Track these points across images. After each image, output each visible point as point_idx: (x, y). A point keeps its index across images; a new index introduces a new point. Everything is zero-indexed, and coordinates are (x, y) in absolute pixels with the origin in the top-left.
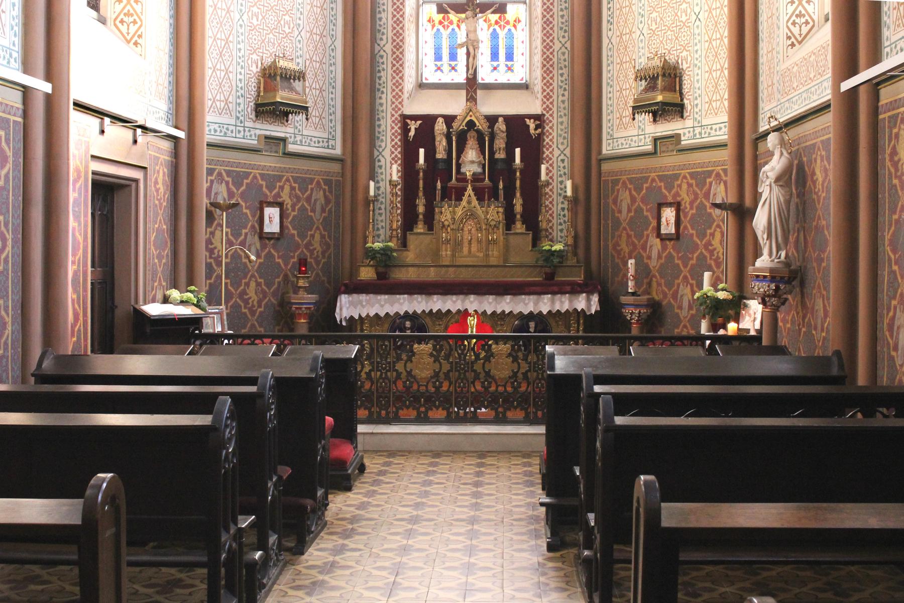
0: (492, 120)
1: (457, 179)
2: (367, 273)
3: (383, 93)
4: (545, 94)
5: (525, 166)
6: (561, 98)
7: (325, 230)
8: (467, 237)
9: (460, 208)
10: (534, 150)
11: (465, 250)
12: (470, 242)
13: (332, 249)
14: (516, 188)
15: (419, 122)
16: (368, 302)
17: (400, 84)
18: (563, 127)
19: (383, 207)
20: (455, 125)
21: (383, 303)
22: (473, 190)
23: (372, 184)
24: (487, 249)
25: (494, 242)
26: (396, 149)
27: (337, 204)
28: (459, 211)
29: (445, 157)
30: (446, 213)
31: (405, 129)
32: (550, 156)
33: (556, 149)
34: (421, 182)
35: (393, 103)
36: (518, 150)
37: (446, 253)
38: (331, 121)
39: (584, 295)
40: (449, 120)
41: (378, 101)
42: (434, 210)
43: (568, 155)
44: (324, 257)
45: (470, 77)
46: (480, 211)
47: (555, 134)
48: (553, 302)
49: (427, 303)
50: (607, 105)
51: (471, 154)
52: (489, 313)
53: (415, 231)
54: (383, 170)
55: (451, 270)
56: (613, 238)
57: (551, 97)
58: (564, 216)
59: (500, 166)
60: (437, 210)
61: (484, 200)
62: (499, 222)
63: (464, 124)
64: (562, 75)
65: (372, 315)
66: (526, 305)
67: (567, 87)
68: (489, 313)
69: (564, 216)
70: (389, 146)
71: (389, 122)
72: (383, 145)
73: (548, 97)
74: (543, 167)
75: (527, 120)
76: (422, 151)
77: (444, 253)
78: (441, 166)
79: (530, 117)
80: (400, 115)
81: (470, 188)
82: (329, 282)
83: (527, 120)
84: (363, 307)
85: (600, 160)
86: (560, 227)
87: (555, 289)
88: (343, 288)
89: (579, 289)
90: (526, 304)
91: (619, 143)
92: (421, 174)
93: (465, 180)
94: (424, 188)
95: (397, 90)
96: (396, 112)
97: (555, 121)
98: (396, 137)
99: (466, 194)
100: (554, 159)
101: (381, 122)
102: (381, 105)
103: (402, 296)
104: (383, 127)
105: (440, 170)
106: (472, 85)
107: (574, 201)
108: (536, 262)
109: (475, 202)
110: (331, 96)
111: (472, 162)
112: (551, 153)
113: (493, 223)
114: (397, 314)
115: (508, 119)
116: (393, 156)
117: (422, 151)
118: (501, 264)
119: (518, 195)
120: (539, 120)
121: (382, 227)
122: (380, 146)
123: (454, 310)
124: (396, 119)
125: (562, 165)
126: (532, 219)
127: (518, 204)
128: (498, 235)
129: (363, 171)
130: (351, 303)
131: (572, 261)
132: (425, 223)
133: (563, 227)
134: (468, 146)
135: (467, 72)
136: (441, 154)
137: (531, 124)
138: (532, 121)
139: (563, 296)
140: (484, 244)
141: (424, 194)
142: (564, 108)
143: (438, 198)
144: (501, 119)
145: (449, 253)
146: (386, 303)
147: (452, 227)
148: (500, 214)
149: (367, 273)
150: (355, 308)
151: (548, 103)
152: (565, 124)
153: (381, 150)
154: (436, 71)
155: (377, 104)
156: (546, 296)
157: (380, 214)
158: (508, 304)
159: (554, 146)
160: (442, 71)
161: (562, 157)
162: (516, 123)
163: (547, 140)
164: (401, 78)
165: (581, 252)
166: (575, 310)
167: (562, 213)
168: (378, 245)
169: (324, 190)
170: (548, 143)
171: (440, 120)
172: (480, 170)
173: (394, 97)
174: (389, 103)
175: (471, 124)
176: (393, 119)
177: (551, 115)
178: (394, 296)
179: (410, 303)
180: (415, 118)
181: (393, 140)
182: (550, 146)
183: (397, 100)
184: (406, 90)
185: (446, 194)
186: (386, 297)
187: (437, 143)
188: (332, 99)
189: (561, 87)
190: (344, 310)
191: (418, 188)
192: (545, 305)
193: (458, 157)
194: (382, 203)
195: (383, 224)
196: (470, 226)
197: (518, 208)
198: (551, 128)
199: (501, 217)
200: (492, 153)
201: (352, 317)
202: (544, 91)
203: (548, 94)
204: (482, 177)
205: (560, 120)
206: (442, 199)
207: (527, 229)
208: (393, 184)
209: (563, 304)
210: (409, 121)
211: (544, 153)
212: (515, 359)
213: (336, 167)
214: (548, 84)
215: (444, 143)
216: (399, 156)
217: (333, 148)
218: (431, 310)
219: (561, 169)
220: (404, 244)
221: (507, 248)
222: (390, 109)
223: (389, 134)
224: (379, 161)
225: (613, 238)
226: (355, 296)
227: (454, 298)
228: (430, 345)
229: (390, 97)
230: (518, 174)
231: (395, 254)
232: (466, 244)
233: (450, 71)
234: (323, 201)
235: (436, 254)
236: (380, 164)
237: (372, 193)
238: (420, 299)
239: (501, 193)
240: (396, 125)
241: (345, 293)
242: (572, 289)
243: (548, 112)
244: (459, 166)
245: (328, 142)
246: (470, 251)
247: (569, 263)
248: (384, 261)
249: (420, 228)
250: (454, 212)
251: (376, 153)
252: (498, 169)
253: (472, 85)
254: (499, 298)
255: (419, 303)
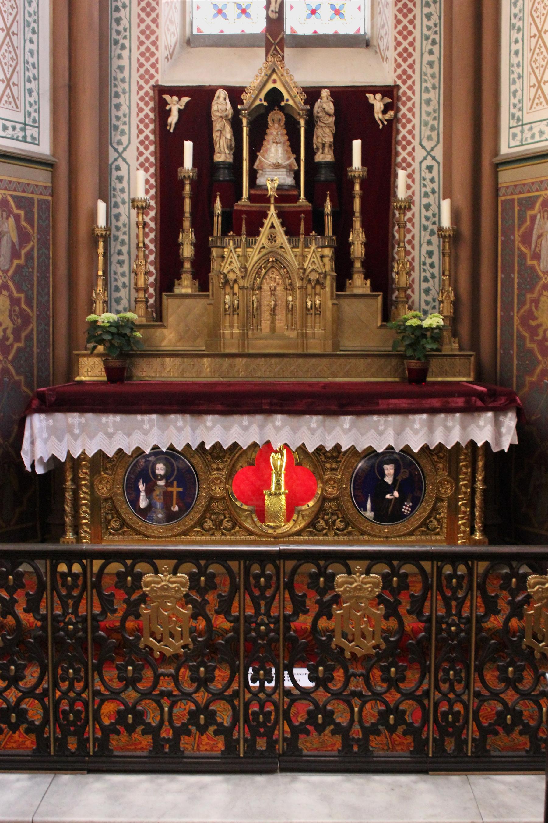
0: (312, 94)
1: (251, 198)
2: (91, 370)
3: (123, 47)
4: (400, 49)
5: (368, 171)
6: (427, 58)
7: (19, 290)
8: (268, 301)
9: (257, 248)
10: (383, 149)
11: (265, 325)
12: (273, 312)
13: (34, 324)
14: (353, 213)
15: (185, 100)
16: (83, 428)
17: (153, 32)
18: (430, 109)
19: (125, 249)
20: (246, 98)
21: (111, 430)
22: (279, 215)
23: (102, 206)
24: (304, 325)
25: (317, 310)
26: (147, 148)
27: (43, 244)
28: (254, 255)
29: (230, 160)
30: (231, 258)
31: (162, 112)
32: (409, 159)
33: (418, 148)
34: (187, 203)
35: (141, 65)
36: (357, 145)
37: (231, 330)
38: (30, 92)
39: (490, 414)
40: (235, 94)
41: (115, 63)
42: (210, 252)
43: (440, 158)
44: (17, 339)
45: (273, 16)
46: (290, 255)
47: (416, 121)
48: (431, 429)
49: (194, 429)
50: (511, 65)
51: (275, 152)
52: (311, 449)
53: (177, 290)
54: (125, 184)
55: (240, 362)
56: (521, 303)
57: (410, 55)
58: (432, 265)
59: (324, 176)
60: (215, 252)
61: (297, 234)
62: (325, 275)
63: (262, 95)
64: (429, 16)
65: (90, 453)
66: (380, 433)
67: (437, 37)
68: (311, 449)
69: (432, 265)
70: (135, 142)
71: (135, 99)
72: (125, 139)
73: (405, 55)
74: (402, 175)
75: (370, 96)
76: (188, 146)
77: (227, 332)
78: (223, 176)
79: (374, 90)
80: (154, 87)
81: (272, 207)
82: (29, 385)
83: (370, 96)
84: (76, 437)
85: (497, 165)
86: (424, 285)
87: (436, 403)
88: (36, 403)
89: (479, 403)
90: (380, 434)
91: (536, 130)
92: (187, 188)
93: (265, 199)
94: (192, 214)
95: (148, 43)
96: (147, 82)
97: (416, 99)
98: (147, 126)
99: (267, 223)
100: (416, 165)
101: (122, 100)
102: (121, 68)
103: (147, 417)
104: (124, 108)
105: (219, 182)
106: (275, 38)
107: (453, 239)
108: (394, 347)
109: (282, 238)
110: (29, 46)
111: (277, 166)
112: (410, 154)
113: (314, 277)
114: (138, 451)
115: (340, 95)
116: (142, 159)
117: (188, 146)
118: (329, 351)
119: (357, 225)
120: (391, 97)
121: (124, 286)
122: (119, 143)
123: (244, 444)
124: (147, 94)
125: (428, 176)
126: (380, 268)
127: (357, 240)
128: (324, 298)
129: (88, 180)
130: (53, 431)
131: (451, 347)
132: (195, 276)
133: (430, 285)
134: (269, 138)
135: (268, 7)
136: (223, 155)
137: (377, 103)
138: (379, 96)
139: (450, 416)
140: (298, 316)
141: (193, 225)
142: (433, 76)
143: (217, 230)
144: (325, 93)
145: (236, 331)
146: (116, 430)
147: (241, 283)
148: (326, 260)
149: (91, 370)
150: (60, 440)
151: (405, 66)
152: (434, 103)
153: (120, 148)
154: (215, 16)
155: (114, 67)
156: (417, 417)
157: (121, 263)
158: (346, 432)
159: (416, 143)
160: (225, 17)
161: (429, 162)
162: (351, 103)
163: (403, 132)
164: (154, 21)
165: (464, 329)
166: (472, 443)
167: (428, 261)
168: (106, 318)
169: (17, 218)
170: (404, 138)
171: (222, 94)
172: (289, 181)
173: (142, 54)
174: (135, 65)
175: (274, 96)
176: (142, 93)
177: (410, 88)
178: (131, 417)
179: (163, 429)
180: (178, 92)
181: (141, 132)
182: (409, 143)
183: (147, 60)
184: (161, 44)
185: (230, 224)
186: (118, 418)
187: (216, 135)
188: (31, 52)
189: (427, 38)
190: (39, 444)
191: (182, 212)
192: (415, 433)
193: (253, 158)
194: (123, 243)
195: (126, 280)
196: (274, 278)
197: (358, 250)
198: (410, 110)
199: (329, 265)
200: (311, 152)
201: (53, 458)
202: (399, 44)
203: (405, 50)
204: (295, 193)
205: (425, 96)
206: (224, 233)
207: (374, 288)
208: (143, 209)
209: (449, 431)
210: (167, 97)
211: (397, 154)
212: (392, 611)
213: (41, 177)
214: (405, 33)
215: (228, 134)
216: (152, 159)
217: (35, 141)
218: (202, 444)
219: (427, 182)
220: (158, 316)
221: (338, 321)
222: (135, 77)
223: (135, 121)
224: (118, 168)
225: (521, 303)
226: (59, 416)
227: (245, 420)
228: (182, 576)
229: (136, 54)
230: (357, 187)
231: (138, 334)
232: (266, 316)
233: (238, 17)
234: (14, 236)
235: (214, 333)
236: (119, 173)
237: (101, 222)
238: (180, 424)
239: (328, 222)
240: (147, 104)
241: (40, 411)
242: (468, 402)
243: (404, 82)
244: (253, 174)
245: (23, 130)
246: (273, 329)
247: (446, 350)
248: (122, 346)
249: (186, 285)
250: (245, 257)
251: (112, 155)
252: (323, 182)
253: (275, 38)
254: (330, 421)
255: (180, 430)
